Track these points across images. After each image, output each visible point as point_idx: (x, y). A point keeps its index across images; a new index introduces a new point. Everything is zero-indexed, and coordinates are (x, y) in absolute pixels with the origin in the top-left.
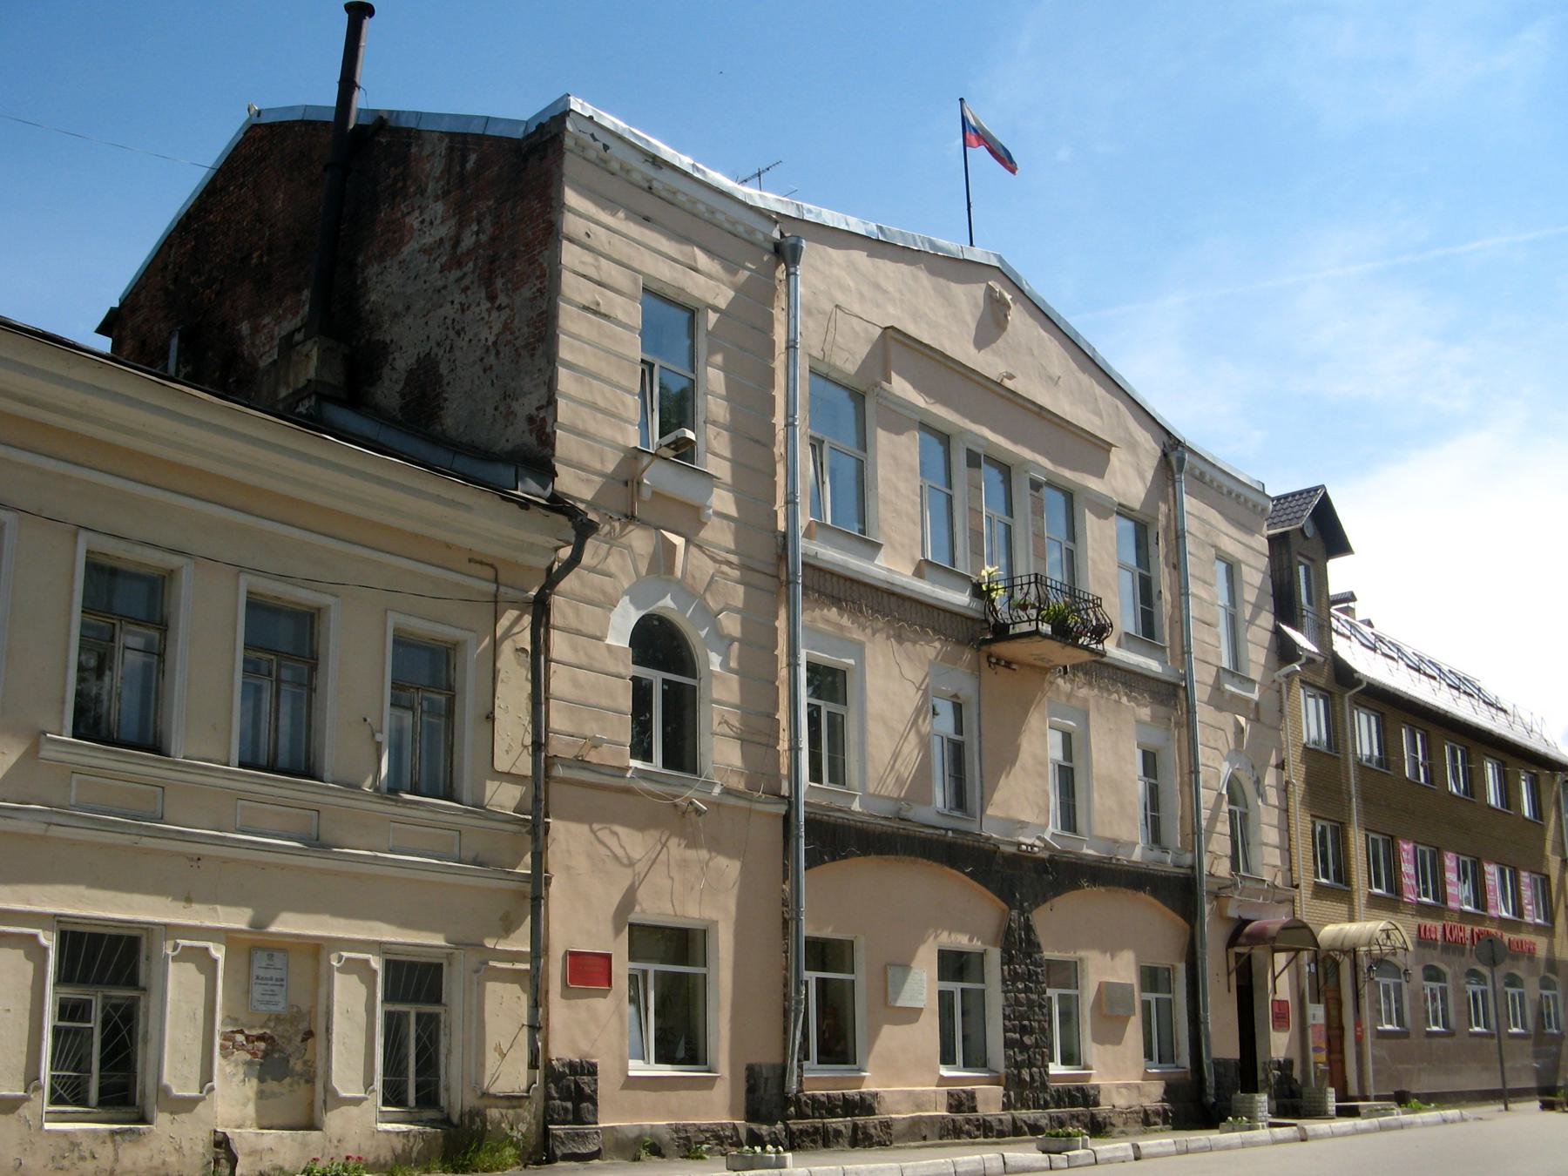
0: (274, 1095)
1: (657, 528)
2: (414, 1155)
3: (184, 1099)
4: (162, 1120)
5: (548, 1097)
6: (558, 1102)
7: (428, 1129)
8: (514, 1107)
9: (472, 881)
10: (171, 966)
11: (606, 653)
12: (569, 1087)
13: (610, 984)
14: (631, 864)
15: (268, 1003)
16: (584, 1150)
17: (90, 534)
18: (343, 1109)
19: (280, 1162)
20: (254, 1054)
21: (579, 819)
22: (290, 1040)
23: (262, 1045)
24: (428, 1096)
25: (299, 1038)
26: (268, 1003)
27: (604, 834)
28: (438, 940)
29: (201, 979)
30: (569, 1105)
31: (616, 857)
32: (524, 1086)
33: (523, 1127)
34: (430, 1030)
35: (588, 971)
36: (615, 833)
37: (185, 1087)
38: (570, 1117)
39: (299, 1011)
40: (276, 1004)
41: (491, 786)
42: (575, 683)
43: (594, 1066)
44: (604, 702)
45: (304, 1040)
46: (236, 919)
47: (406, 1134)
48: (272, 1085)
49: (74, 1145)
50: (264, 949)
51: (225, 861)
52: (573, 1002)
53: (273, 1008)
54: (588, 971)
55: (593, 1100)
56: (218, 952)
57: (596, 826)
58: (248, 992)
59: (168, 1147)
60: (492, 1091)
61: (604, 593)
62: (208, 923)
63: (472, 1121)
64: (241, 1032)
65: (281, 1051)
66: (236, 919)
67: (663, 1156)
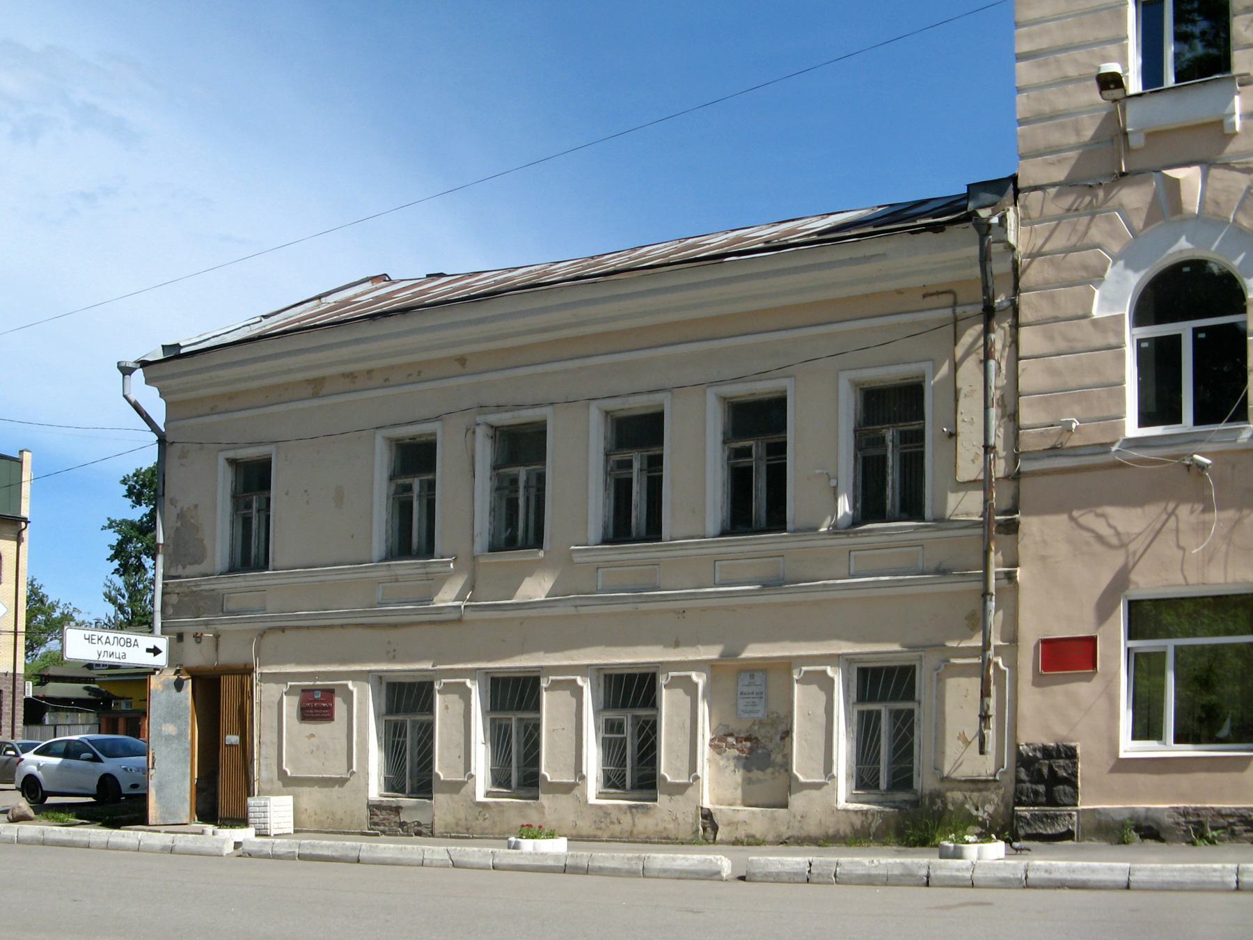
0: (759, 781)
1: (1158, 171)
2: (873, 829)
3: (678, 785)
4: (662, 798)
5: (1018, 781)
6: (1028, 785)
7: (887, 810)
8: (980, 790)
9: (929, 589)
10: (796, 686)
11: (1091, 329)
12: (1040, 771)
13: (1095, 666)
14: (1123, 545)
15: (751, 712)
16: (1050, 831)
17: (597, 402)
18: (806, 792)
19: (753, 832)
20: (742, 751)
21: (1056, 509)
22: (771, 740)
23: (748, 744)
24: (902, 779)
25: (778, 738)
26: (751, 712)
27: (1088, 519)
28: (896, 647)
29: (822, 697)
30: (1041, 788)
31: (1100, 539)
32: (991, 770)
33: (990, 808)
34: (905, 724)
35: (1068, 657)
36: (1103, 516)
37: (678, 776)
38: (1043, 799)
39: (778, 717)
40: (757, 712)
41: (953, 499)
42: (1053, 372)
43: (1073, 749)
44: (1088, 380)
45: (782, 738)
46: (711, 653)
47: (864, 813)
48: (757, 774)
49: (607, 814)
50: (746, 671)
51: (704, 610)
52: (1047, 689)
53: (755, 715)
54: (1068, 657)
55: (1071, 781)
56: (699, 679)
57: (1075, 514)
58: (736, 705)
59: (667, 818)
60: (954, 775)
61: (1086, 268)
62: (691, 658)
63: (933, 802)
64: (731, 735)
65: (764, 747)
66: (711, 653)
67: (1163, 841)
